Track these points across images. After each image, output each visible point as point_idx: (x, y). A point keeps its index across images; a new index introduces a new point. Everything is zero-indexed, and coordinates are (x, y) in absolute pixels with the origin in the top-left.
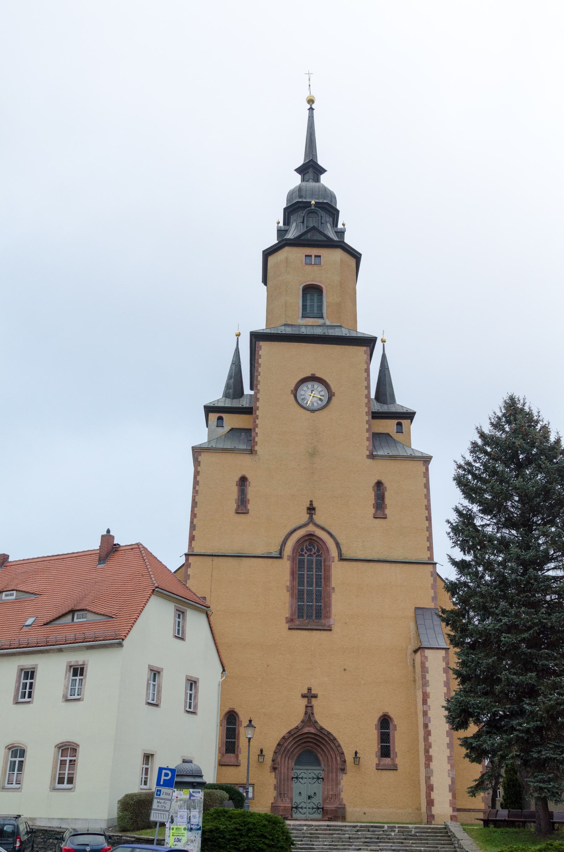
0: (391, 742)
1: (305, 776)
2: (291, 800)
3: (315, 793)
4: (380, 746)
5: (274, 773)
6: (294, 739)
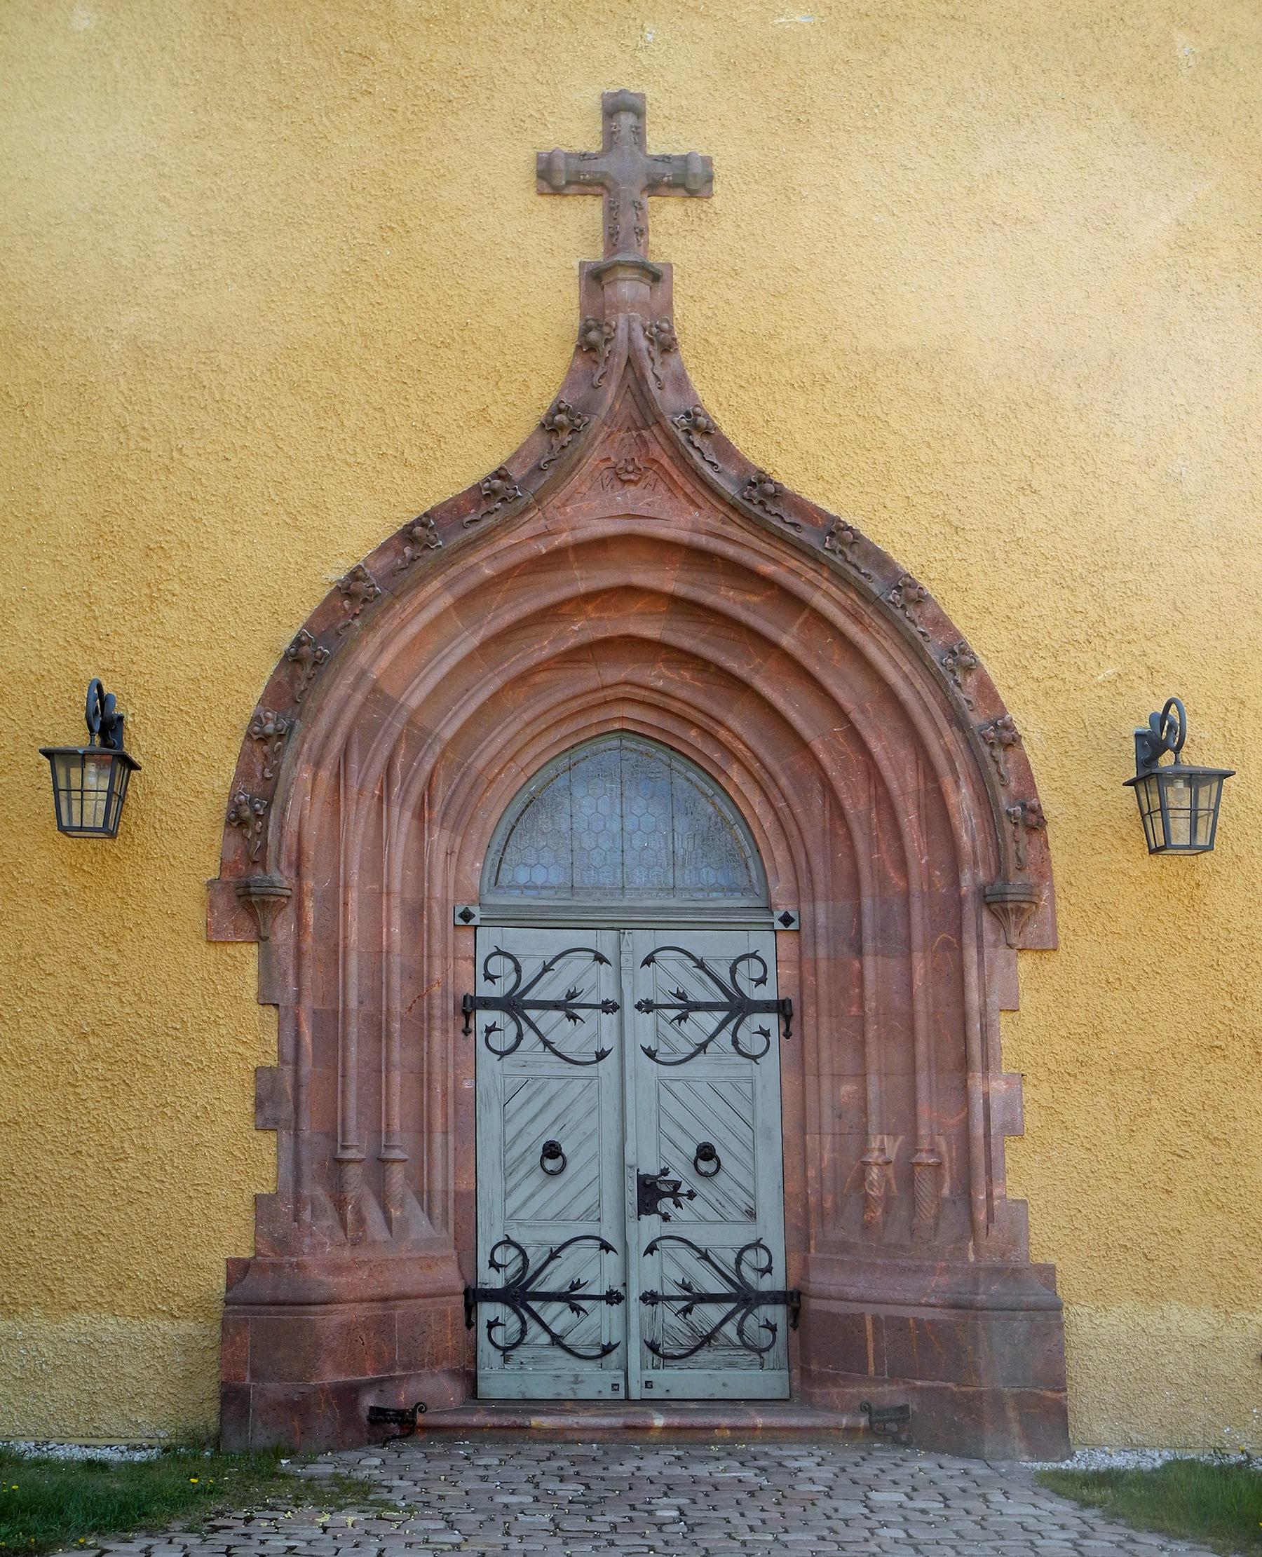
3: (706, 1152)
5: (250, 954)
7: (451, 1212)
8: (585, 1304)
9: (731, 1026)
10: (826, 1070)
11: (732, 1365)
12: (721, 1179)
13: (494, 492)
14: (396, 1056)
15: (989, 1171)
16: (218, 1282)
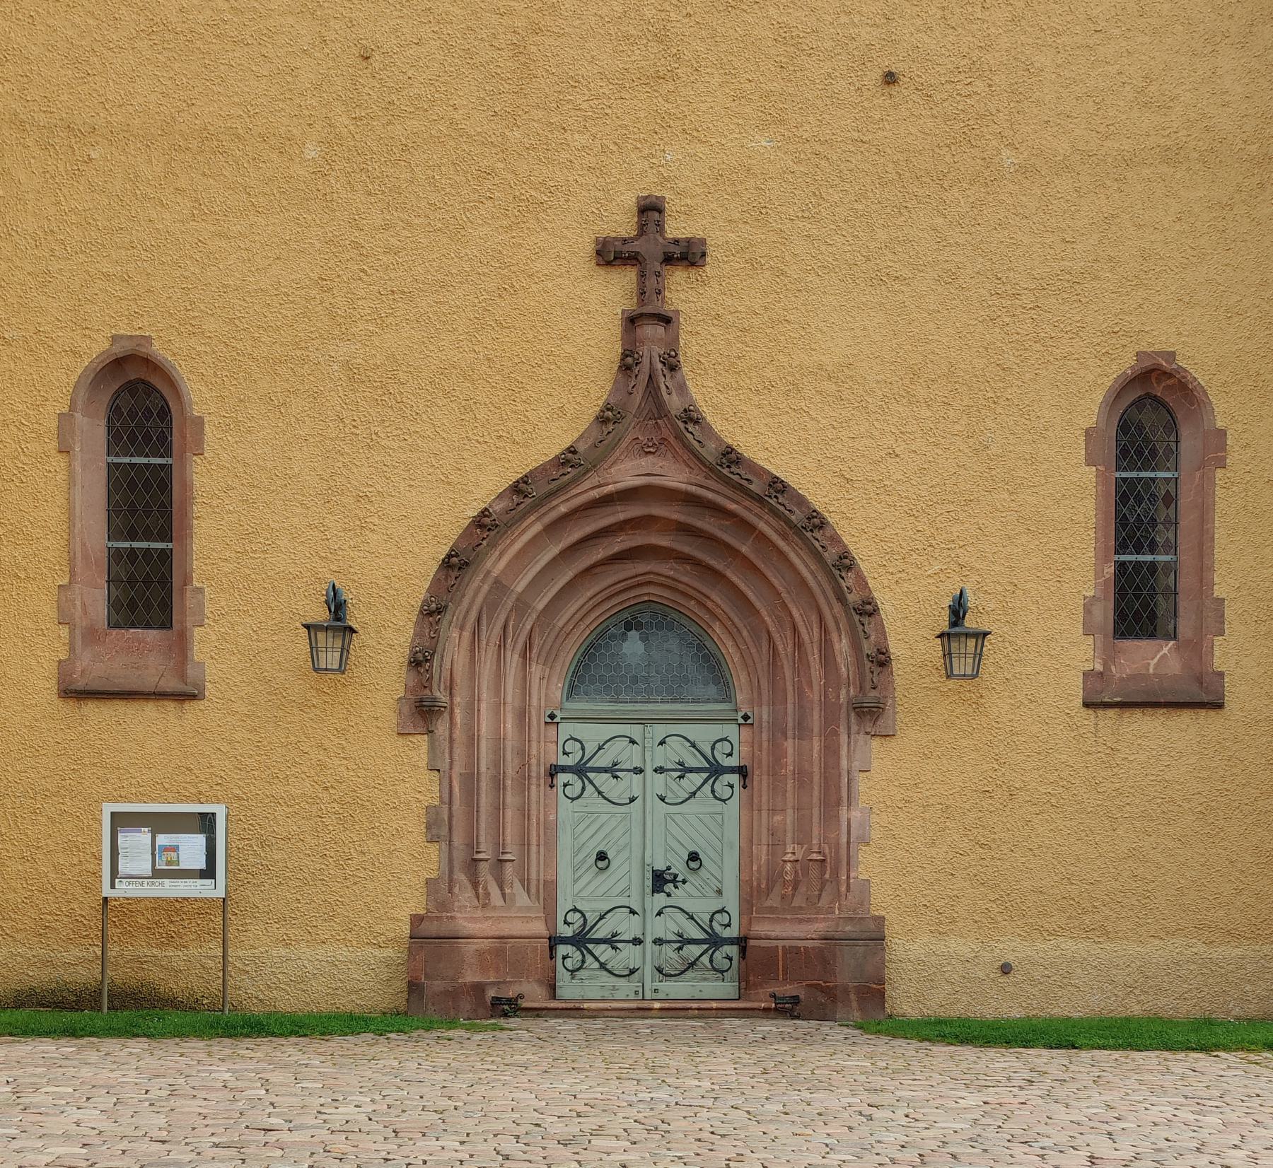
0: (1186, 544)
1: (631, 756)
3: (694, 857)
4: (1110, 570)
7: (541, 891)
8: (619, 945)
10: (765, 807)
11: (705, 980)
12: (702, 872)
13: (568, 461)
14: (509, 799)
15: (848, 864)
16: (406, 930)
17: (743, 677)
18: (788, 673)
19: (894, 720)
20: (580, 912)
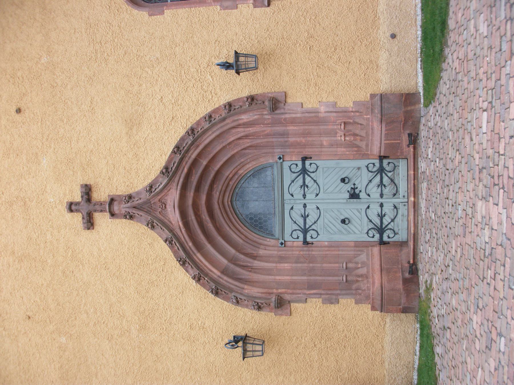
1: (299, 208)
2: (360, 245)
3: (343, 180)
6: (199, 247)
8: (383, 213)
9: (309, 173)
11: (399, 174)
16: (378, 313)
17: (262, 160)
18: (259, 141)
19: (278, 92)
20: (368, 231)
